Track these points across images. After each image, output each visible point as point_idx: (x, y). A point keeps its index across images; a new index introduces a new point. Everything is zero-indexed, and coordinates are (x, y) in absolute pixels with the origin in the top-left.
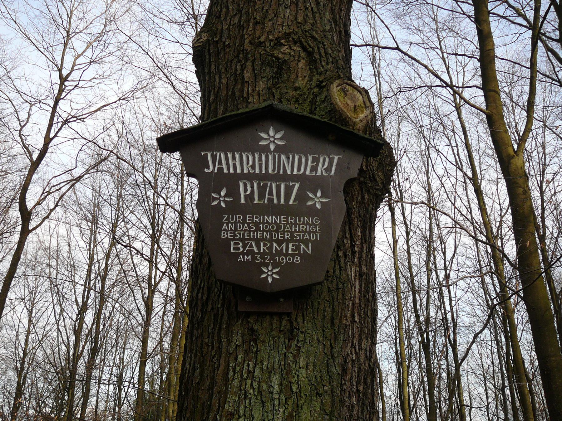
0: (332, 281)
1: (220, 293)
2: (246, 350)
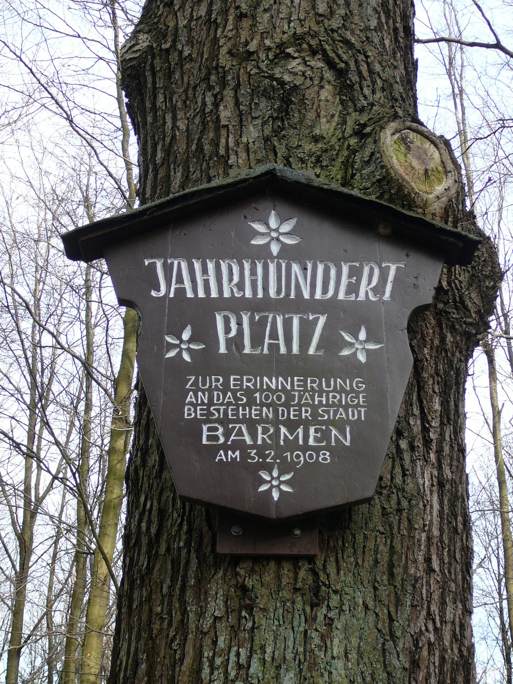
0: (389, 496)
1: (182, 520)
2: (232, 627)
